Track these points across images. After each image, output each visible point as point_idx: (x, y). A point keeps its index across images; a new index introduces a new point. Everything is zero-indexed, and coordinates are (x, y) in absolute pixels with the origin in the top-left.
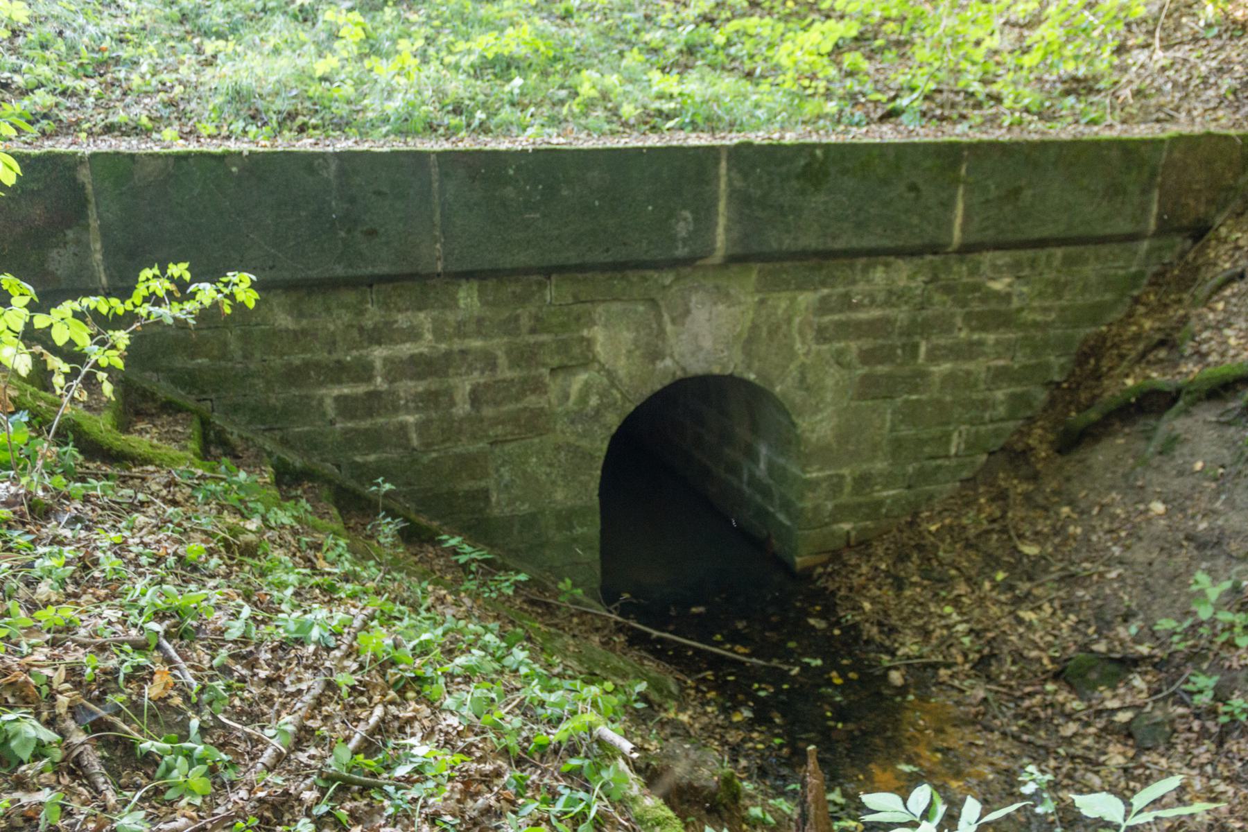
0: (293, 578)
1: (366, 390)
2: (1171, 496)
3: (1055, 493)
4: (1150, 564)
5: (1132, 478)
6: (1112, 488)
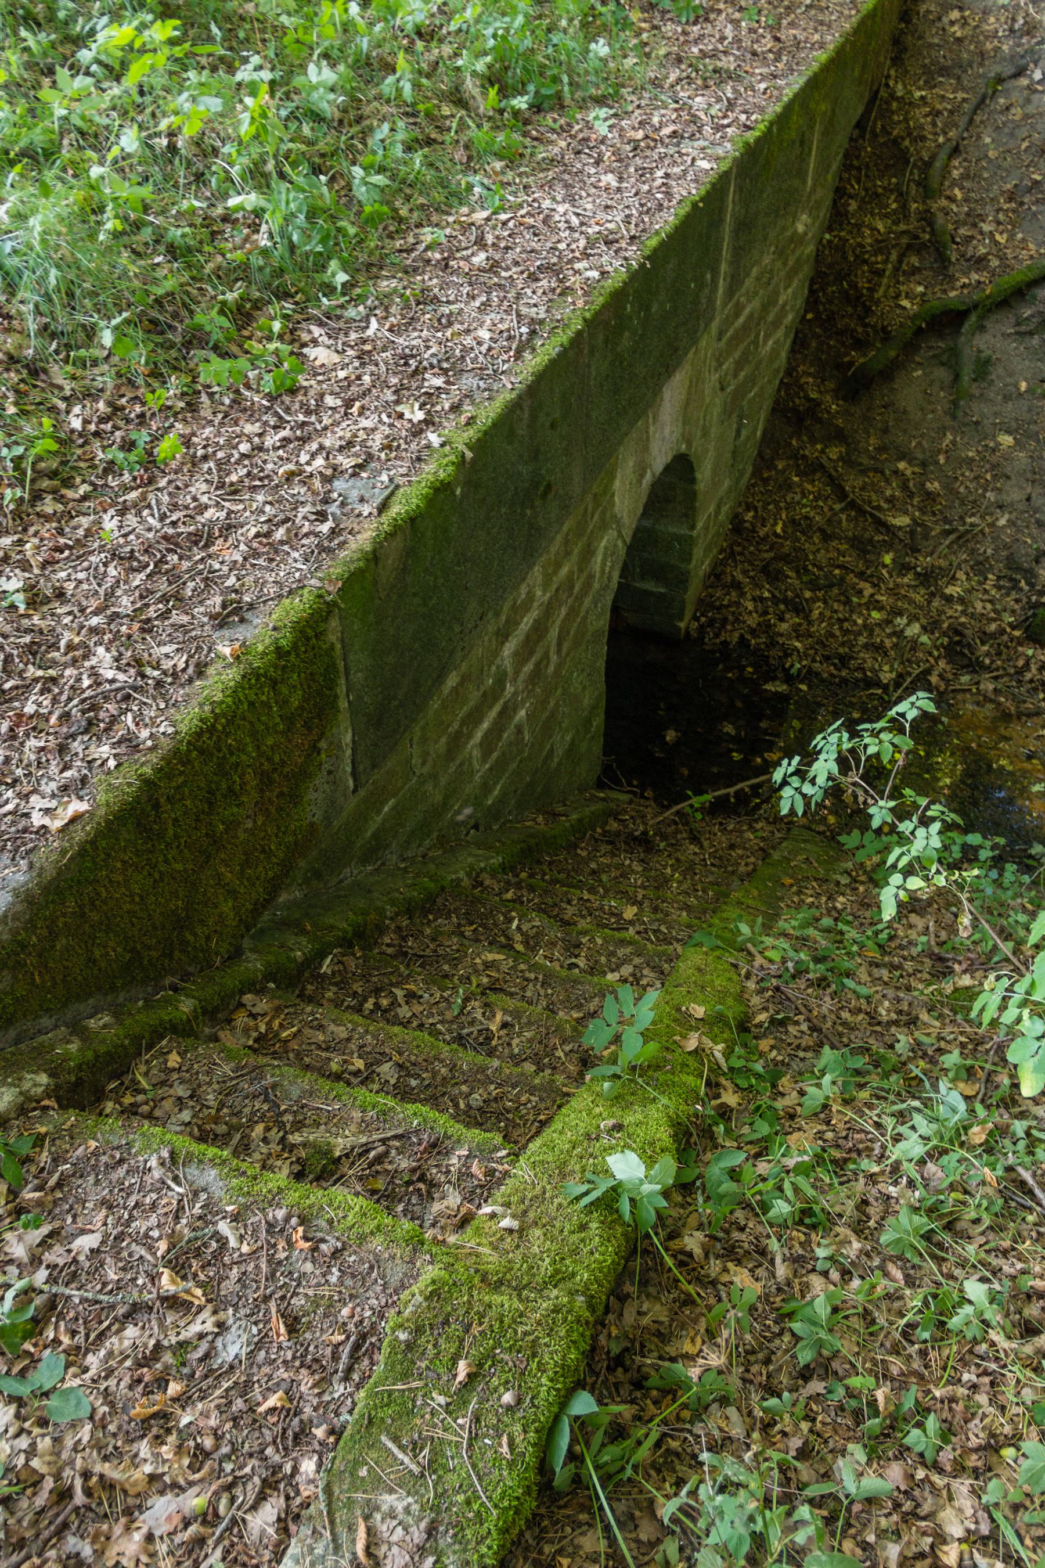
0: (199, 487)
1: (522, 626)
2: (1014, 425)
3: (882, 449)
4: (1028, 499)
5: (960, 414)
6: (944, 429)
